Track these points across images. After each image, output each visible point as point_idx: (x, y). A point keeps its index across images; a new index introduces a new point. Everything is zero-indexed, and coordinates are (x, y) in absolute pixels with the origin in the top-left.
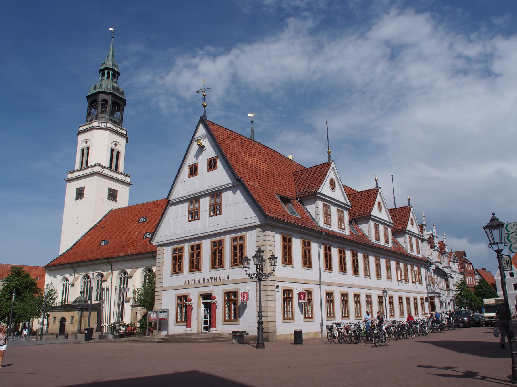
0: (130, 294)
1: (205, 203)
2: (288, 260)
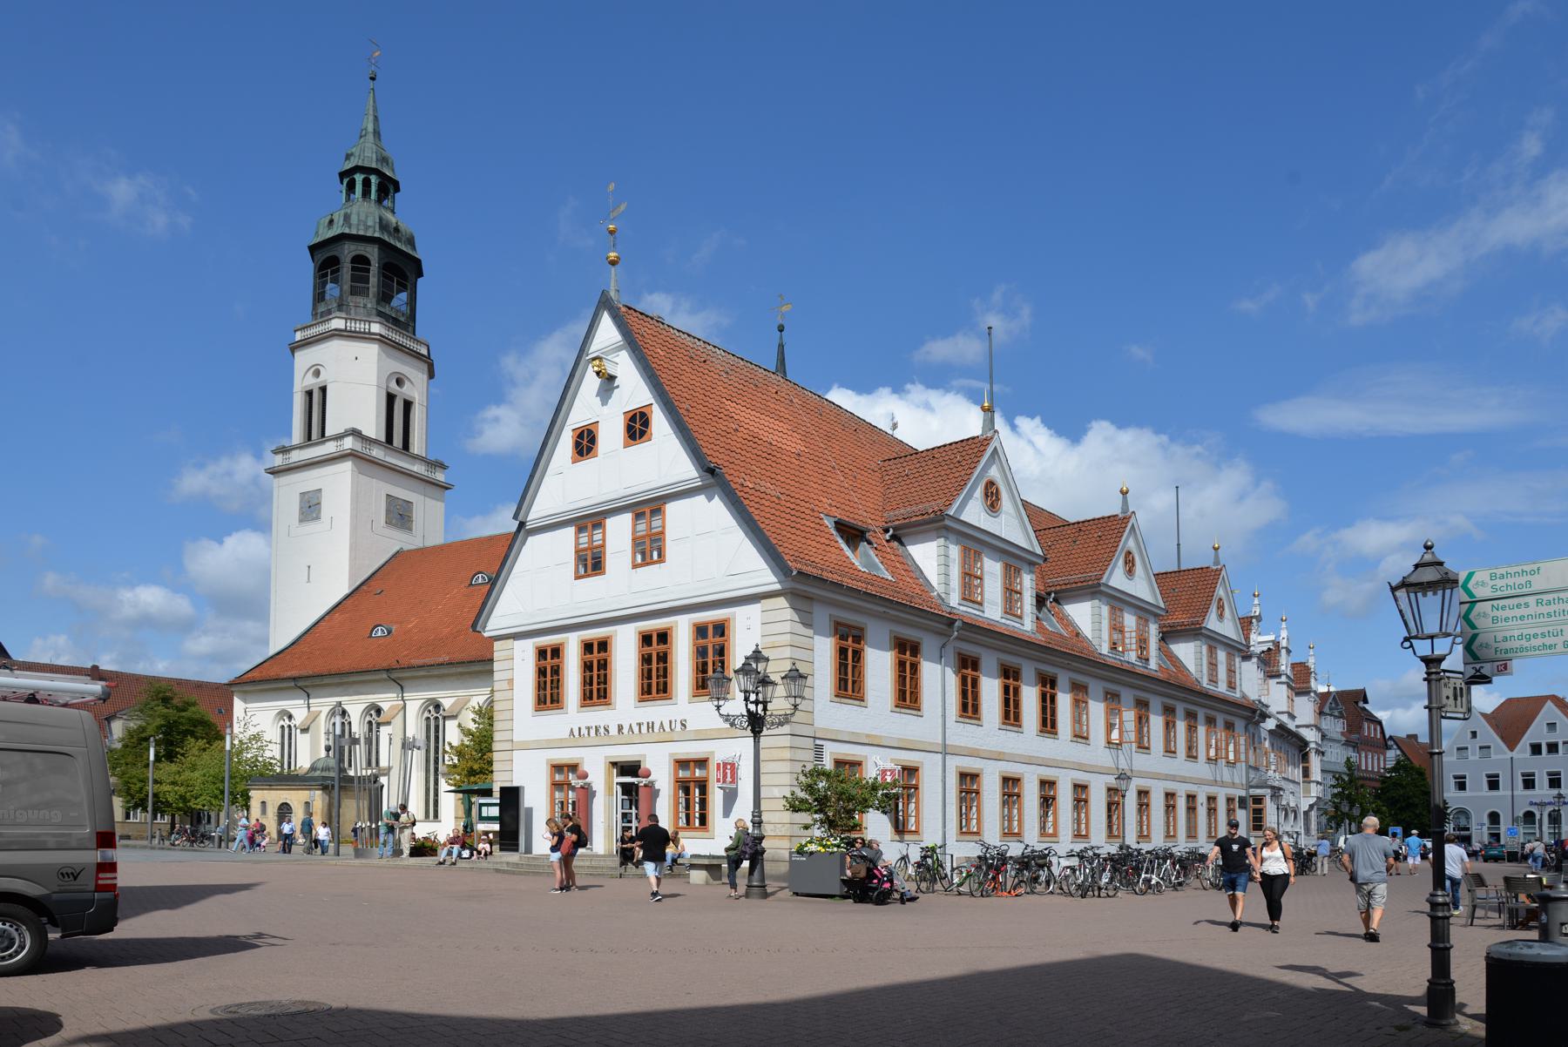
0: (451, 759)
1: (619, 532)
2: (849, 684)
